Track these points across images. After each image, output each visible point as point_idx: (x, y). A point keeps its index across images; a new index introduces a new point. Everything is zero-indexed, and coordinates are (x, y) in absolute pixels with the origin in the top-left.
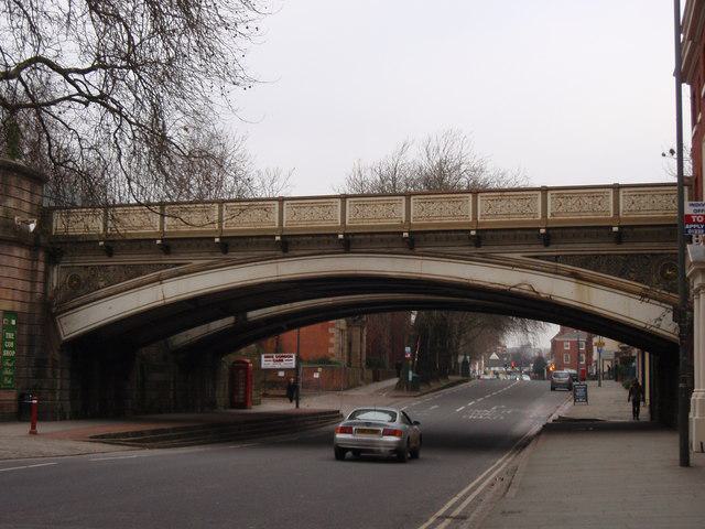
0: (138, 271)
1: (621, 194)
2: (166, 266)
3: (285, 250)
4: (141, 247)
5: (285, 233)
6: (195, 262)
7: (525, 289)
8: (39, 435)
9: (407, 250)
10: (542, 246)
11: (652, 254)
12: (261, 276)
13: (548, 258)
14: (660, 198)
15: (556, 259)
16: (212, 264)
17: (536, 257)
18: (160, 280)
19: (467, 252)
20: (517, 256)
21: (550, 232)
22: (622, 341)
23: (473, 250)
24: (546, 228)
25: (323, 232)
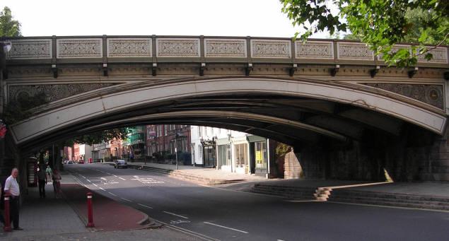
0: (80, 88)
1: (157, 42)
2: (105, 85)
3: (201, 74)
4: (433, 73)
5: (58, 62)
6: (128, 82)
7: (360, 104)
8: (22, 230)
9: (288, 77)
10: (53, 78)
11: (426, 85)
12: (320, 93)
13: (372, 85)
14: (84, 46)
15: (377, 85)
16: (143, 83)
17: (365, 84)
18: (100, 95)
19: (325, 79)
20: (355, 83)
21: (160, 65)
22: (248, 132)
23: (330, 78)
24: (157, 63)
25: (363, 64)
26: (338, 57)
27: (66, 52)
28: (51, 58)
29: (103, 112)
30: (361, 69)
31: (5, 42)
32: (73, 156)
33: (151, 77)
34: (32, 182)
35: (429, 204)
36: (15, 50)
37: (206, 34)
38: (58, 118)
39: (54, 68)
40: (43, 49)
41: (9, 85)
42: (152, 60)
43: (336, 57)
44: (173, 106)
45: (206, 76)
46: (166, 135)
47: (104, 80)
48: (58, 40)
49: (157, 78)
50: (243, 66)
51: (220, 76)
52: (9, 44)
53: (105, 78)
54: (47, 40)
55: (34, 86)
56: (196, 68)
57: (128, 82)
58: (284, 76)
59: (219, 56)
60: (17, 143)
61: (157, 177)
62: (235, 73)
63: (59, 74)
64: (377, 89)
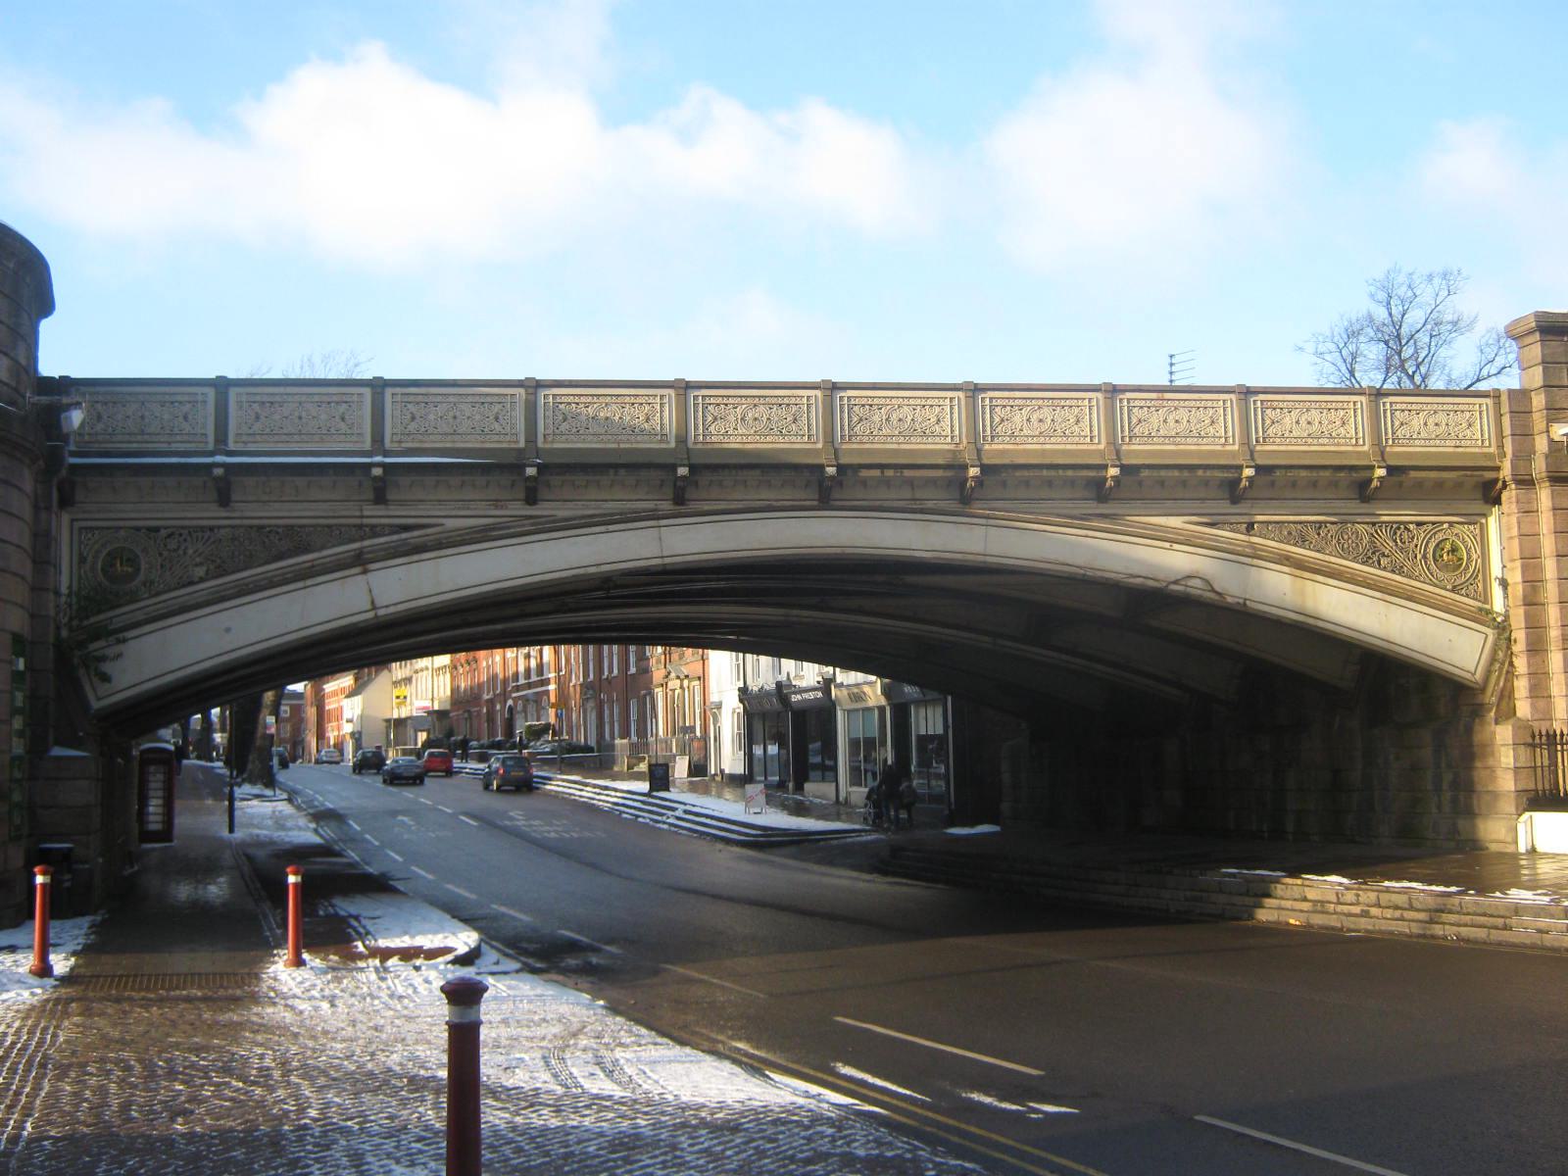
18: (361, 562)
27: (257, 428)
28: (522, 444)
29: (371, 615)
31: (65, 400)
32: (321, 735)
34: (153, 827)
36: (99, 418)
37: (232, 375)
38: (228, 630)
39: (530, 478)
40: (186, 418)
41: (77, 525)
42: (530, 459)
44: (599, 593)
45: (693, 506)
46: (633, 670)
47: (375, 514)
48: (389, 392)
49: (541, 510)
50: (949, 473)
51: (740, 505)
52: (78, 405)
53: (380, 510)
55: (157, 529)
56: (949, 483)
57: (451, 523)
58: (942, 504)
59: (1448, 447)
60: (96, 705)
63: (235, 497)
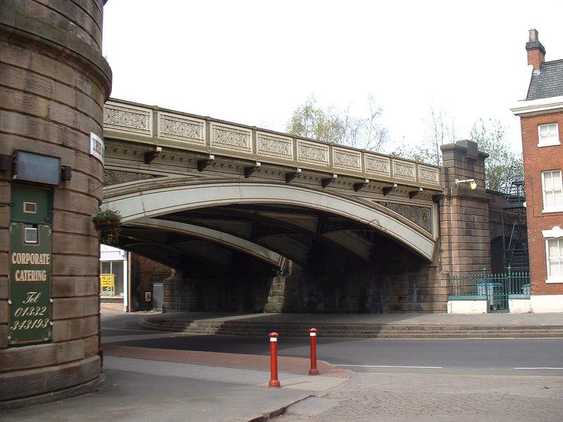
2: (143, 176)
9: (321, 188)
17: (378, 202)
19: (348, 194)
20: (370, 200)
23: (353, 193)
26: (159, 134)
29: (143, 215)
30: (130, 149)
33: (195, 172)
35: (548, 332)
37: (161, 106)
43: (155, 134)
45: (250, 179)
51: (267, 180)
53: (144, 166)
54: (148, 110)
61: (117, 313)
62: (276, 178)
64: (385, 208)
